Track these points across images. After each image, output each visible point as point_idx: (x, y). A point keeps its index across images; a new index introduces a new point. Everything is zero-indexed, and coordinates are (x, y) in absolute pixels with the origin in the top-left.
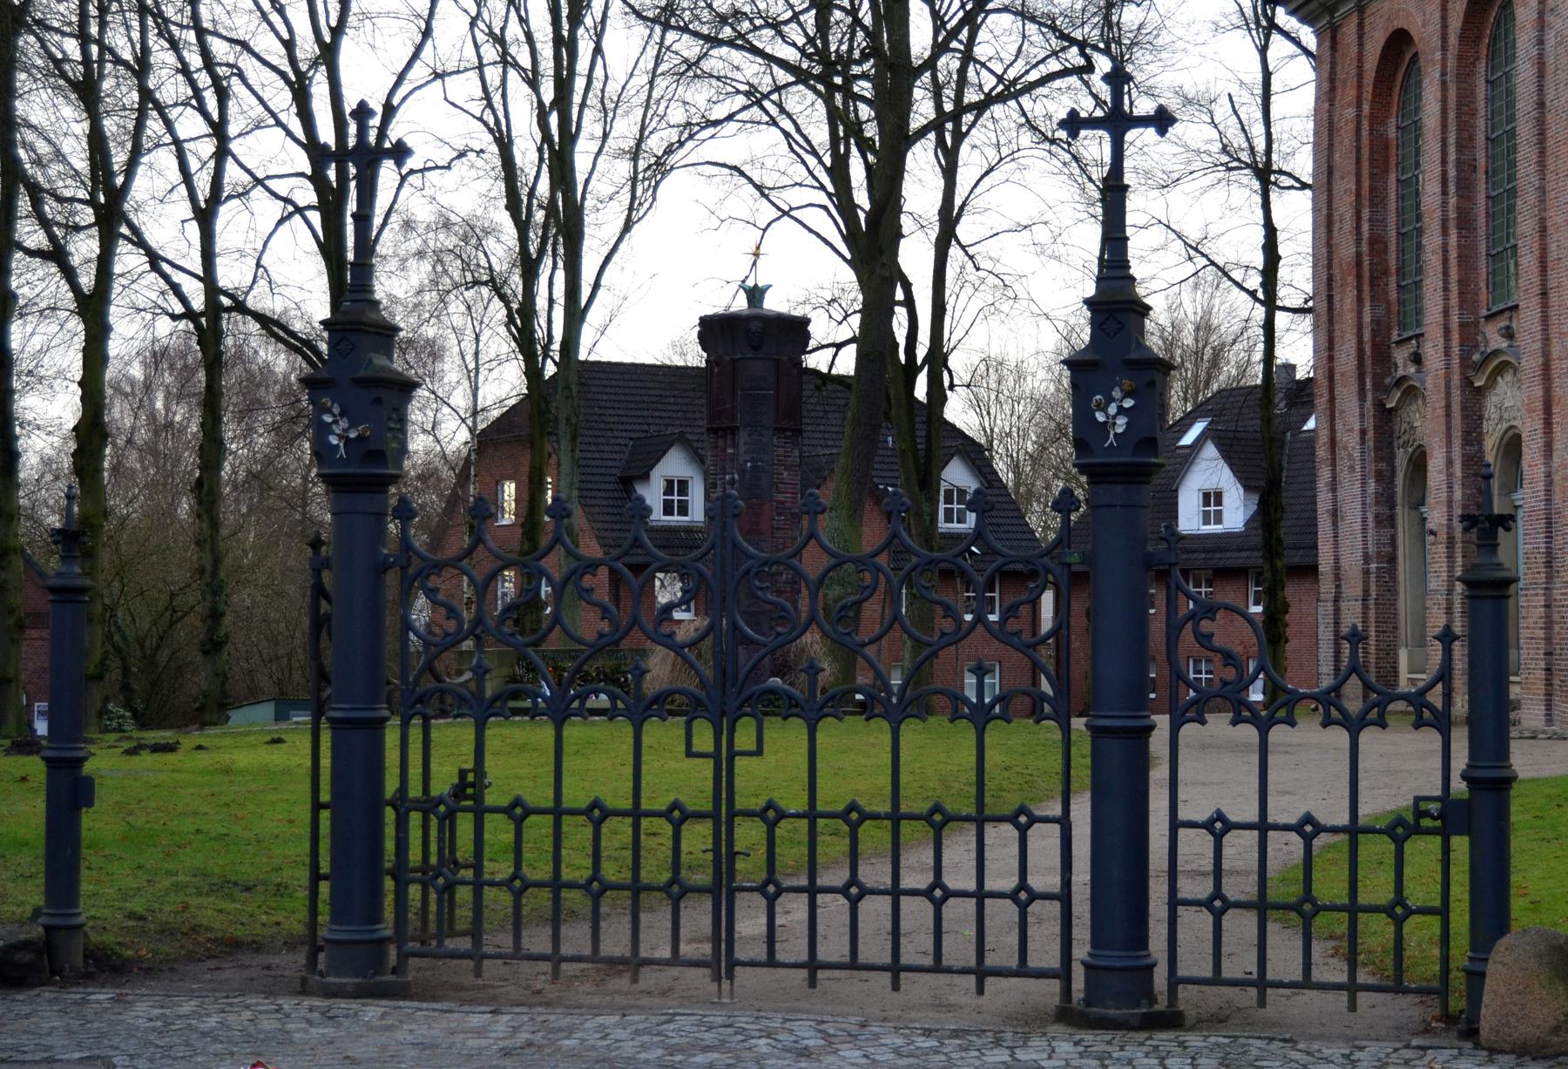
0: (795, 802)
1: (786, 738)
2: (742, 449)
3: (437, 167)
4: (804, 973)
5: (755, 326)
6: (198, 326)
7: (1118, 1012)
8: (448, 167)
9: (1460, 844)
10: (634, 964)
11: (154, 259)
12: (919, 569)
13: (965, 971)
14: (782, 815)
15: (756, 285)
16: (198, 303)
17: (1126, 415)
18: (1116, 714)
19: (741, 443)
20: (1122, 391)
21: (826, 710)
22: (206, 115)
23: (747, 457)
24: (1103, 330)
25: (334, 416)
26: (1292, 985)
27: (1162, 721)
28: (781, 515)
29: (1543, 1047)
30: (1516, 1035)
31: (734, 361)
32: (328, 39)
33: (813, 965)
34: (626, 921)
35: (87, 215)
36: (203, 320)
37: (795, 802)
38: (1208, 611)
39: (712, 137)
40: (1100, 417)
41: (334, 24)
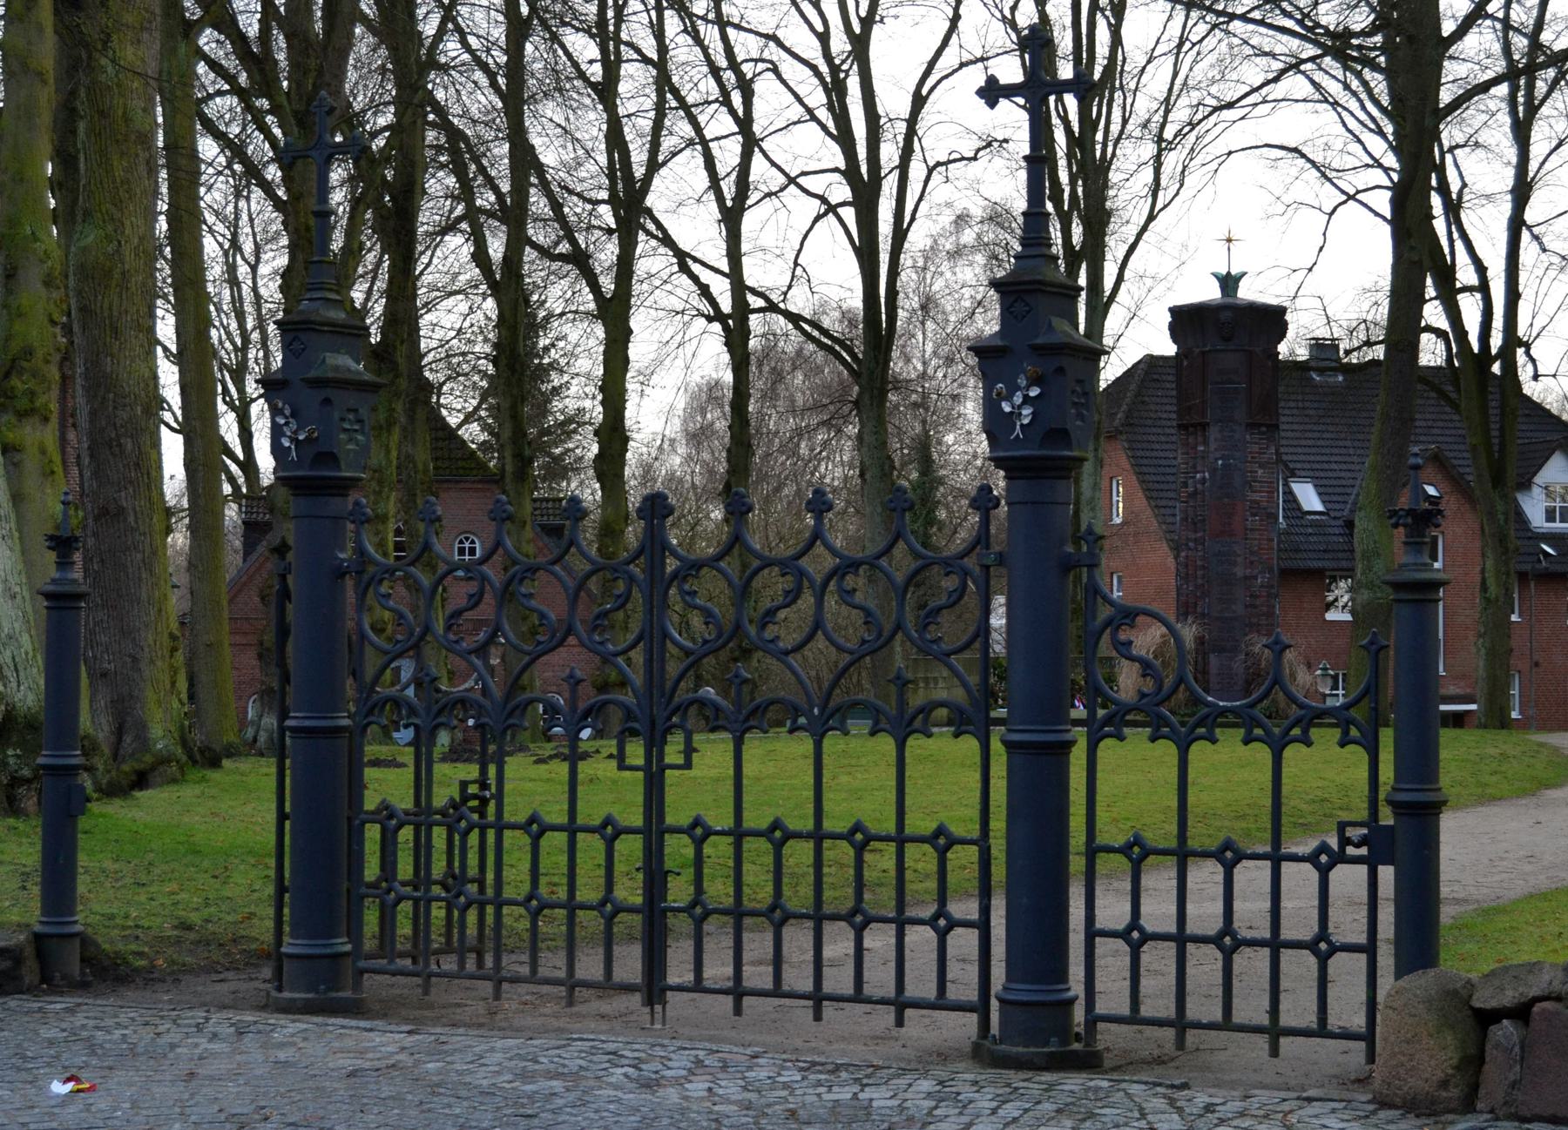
0: (721, 818)
1: (714, 753)
2: (1213, 446)
3: (963, 159)
4: (729, 1000)
5: (1228, 314)
6: (726, 328)
7: (1026, 1050)
8: (975, 158)
9: (1386, 873)
10: (572, 985)
11: (683, 259)
12: (840, 573)
13: (883, 1002)
14: (709, 832)
15: (1229, 273)
16: (726, 305)
17: (1032, 405)
18: (1021, 727)
19: (1212, 439)
20: (1027, 379)
21: (752, 723)
22: (733, 112)
23: (1218, 455)
24: (1011, 313)
25: (286, 417)
26: (1211, 1026)
27: (1080, 735)
28: (1254, 515)
29: (1433, 1103)
30: (1406, 1089)
31: (1203, 353)
32: (857, 30)
33: (738, 992)
34: (729, 942)
35: (606, 215)
36: (730, 322)
37: (721, 818)
38: (1126, 617)
39: (1243, 118)
40: (1007, 408)
41: (863, 14)
